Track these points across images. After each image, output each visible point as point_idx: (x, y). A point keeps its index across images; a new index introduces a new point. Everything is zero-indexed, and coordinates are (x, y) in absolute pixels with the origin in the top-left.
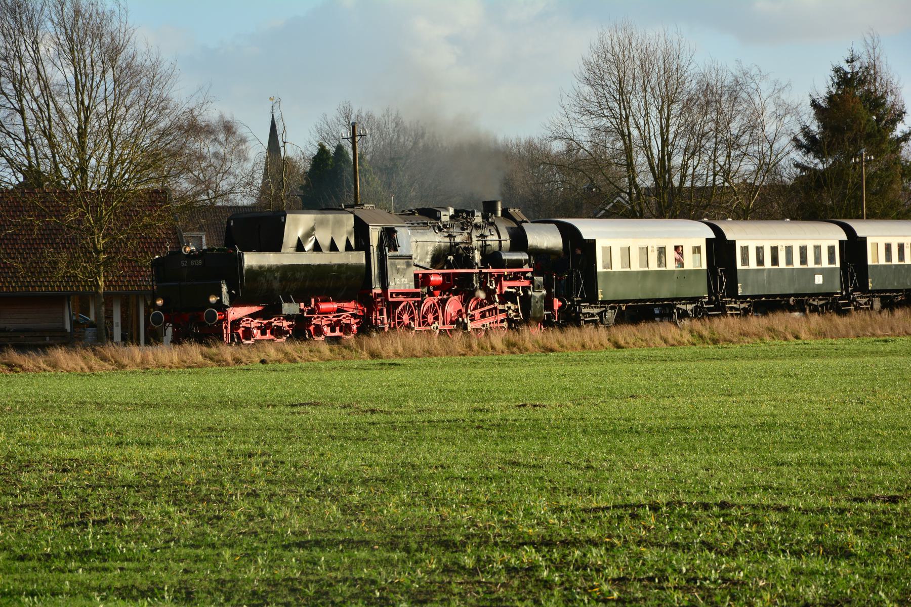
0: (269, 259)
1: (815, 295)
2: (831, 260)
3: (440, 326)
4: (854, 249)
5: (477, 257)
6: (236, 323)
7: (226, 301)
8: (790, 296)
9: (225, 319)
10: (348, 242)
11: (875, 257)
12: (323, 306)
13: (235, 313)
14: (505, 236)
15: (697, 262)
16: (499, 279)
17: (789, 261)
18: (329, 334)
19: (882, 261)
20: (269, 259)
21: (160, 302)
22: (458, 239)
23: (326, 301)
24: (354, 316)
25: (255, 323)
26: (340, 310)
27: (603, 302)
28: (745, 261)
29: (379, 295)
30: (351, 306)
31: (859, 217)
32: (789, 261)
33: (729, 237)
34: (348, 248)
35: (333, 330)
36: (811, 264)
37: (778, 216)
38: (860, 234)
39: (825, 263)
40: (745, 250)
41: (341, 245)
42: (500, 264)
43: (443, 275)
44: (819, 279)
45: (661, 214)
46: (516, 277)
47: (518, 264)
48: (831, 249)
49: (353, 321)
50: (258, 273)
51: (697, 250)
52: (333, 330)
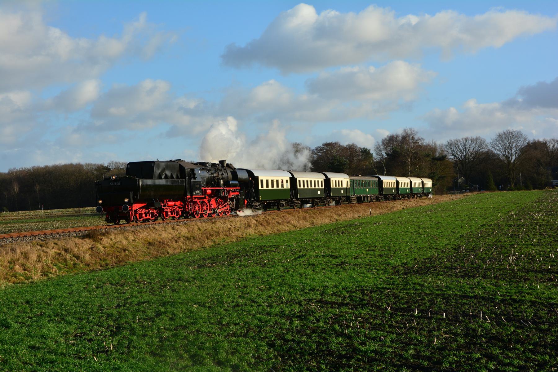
0: (149, 182)
1: (317, 198)
2: (322, 186)
3: (208, 212)
4: (327, 181)
5: (222, 182)
6: (136, 211)
7: (132, 201)
8: (310, 198)
9: (131, 210)
10: (177, 175)
11: (333, 185)
12: (169, 203)
13: (135, 207)
14: (230, 174)
15: (287, 186)
16: (229, 191)
17: (267, 186)
18: (145, 218)
19: (334, 187)
20: (149, 182)
21: (100, 202)
22: (215, 175)
23: (170, 201)
24: (179, 207)
25: (143, 211)
26: (175, 205)
27: (261, 201)
28: (262, 186)
29: (189, 198)
30: (178, 203)
31: (383, 175)
32: (267, 186)
33: (295, 177)
34: (177, 178)
35: (146, 216)
36: (317, 187)
37: (493, 186)
38: (329, 177)
39: (320, 187)
40: (262, 181)
41: (175, 176)
42: (230, 186)
43: (211, 190)
44: (319, 192)
45: (527, 188)
46: (234, 191)
47: (235, 186)
48: (322, 182)
49: (180, 210)
50: (146, 188)
51: (287, 181)
52: (146, 216)
